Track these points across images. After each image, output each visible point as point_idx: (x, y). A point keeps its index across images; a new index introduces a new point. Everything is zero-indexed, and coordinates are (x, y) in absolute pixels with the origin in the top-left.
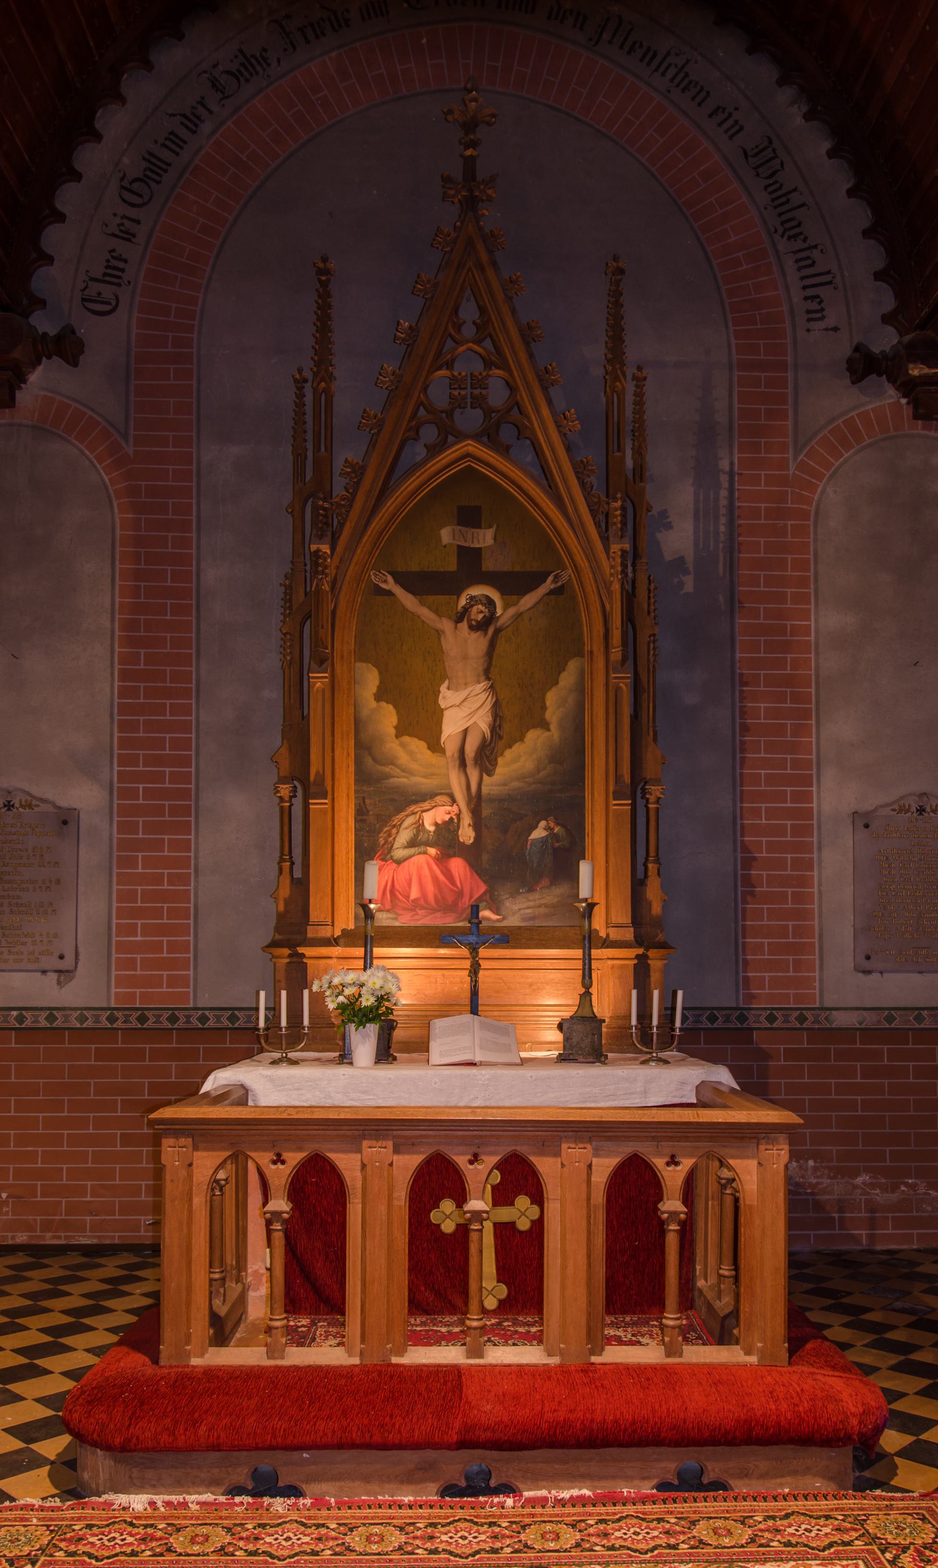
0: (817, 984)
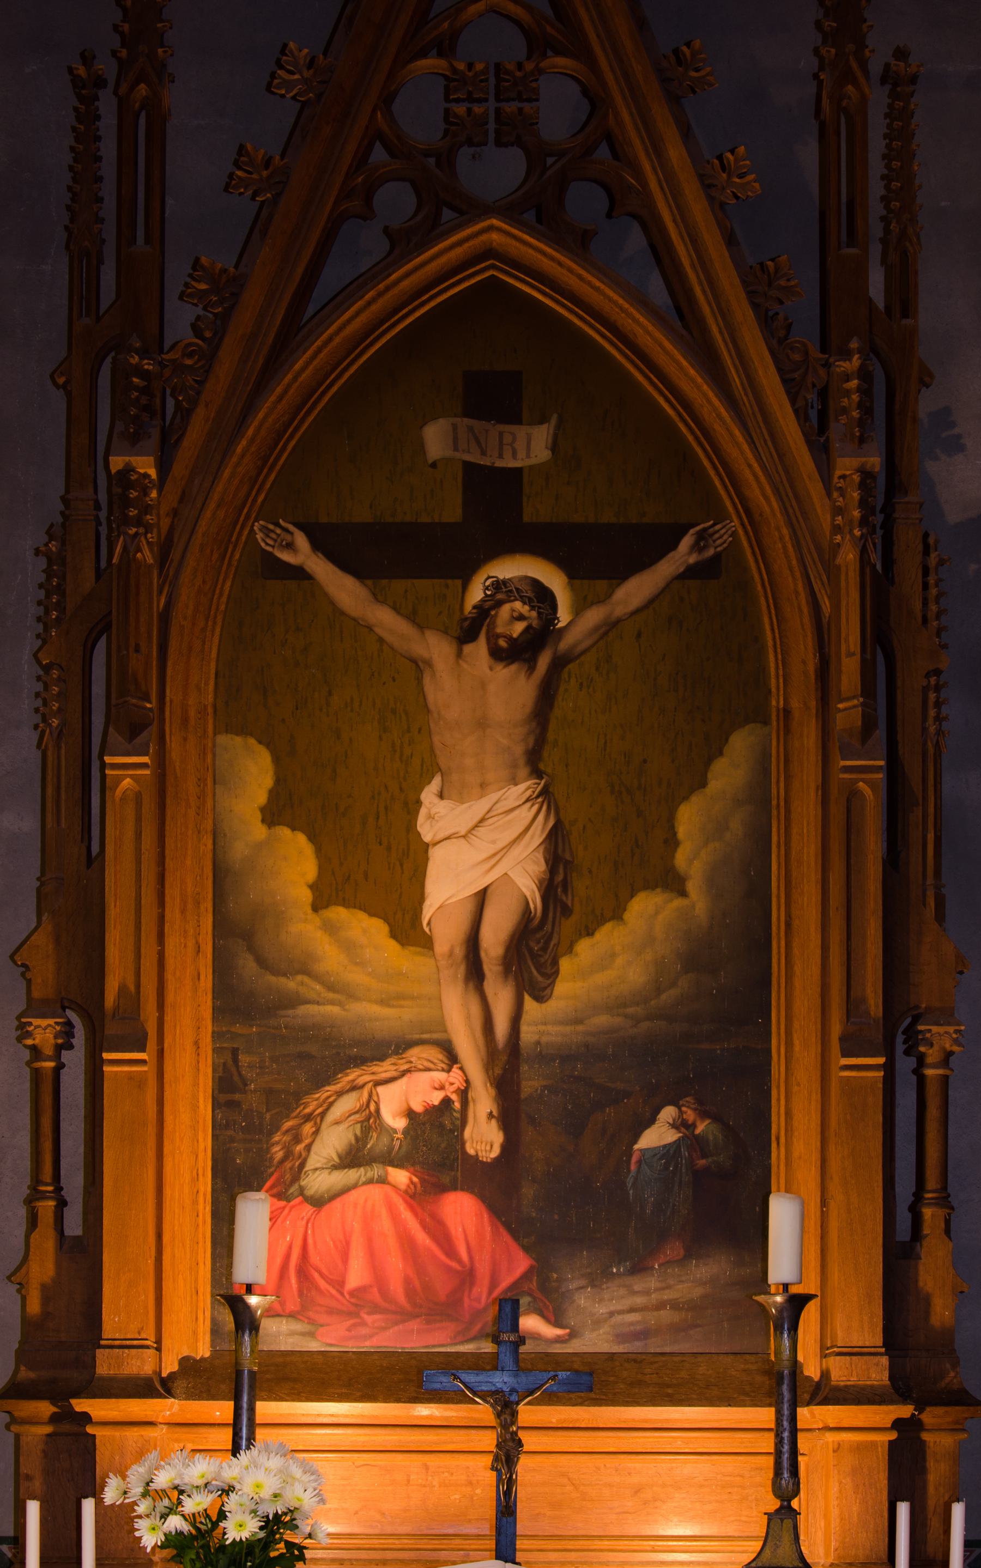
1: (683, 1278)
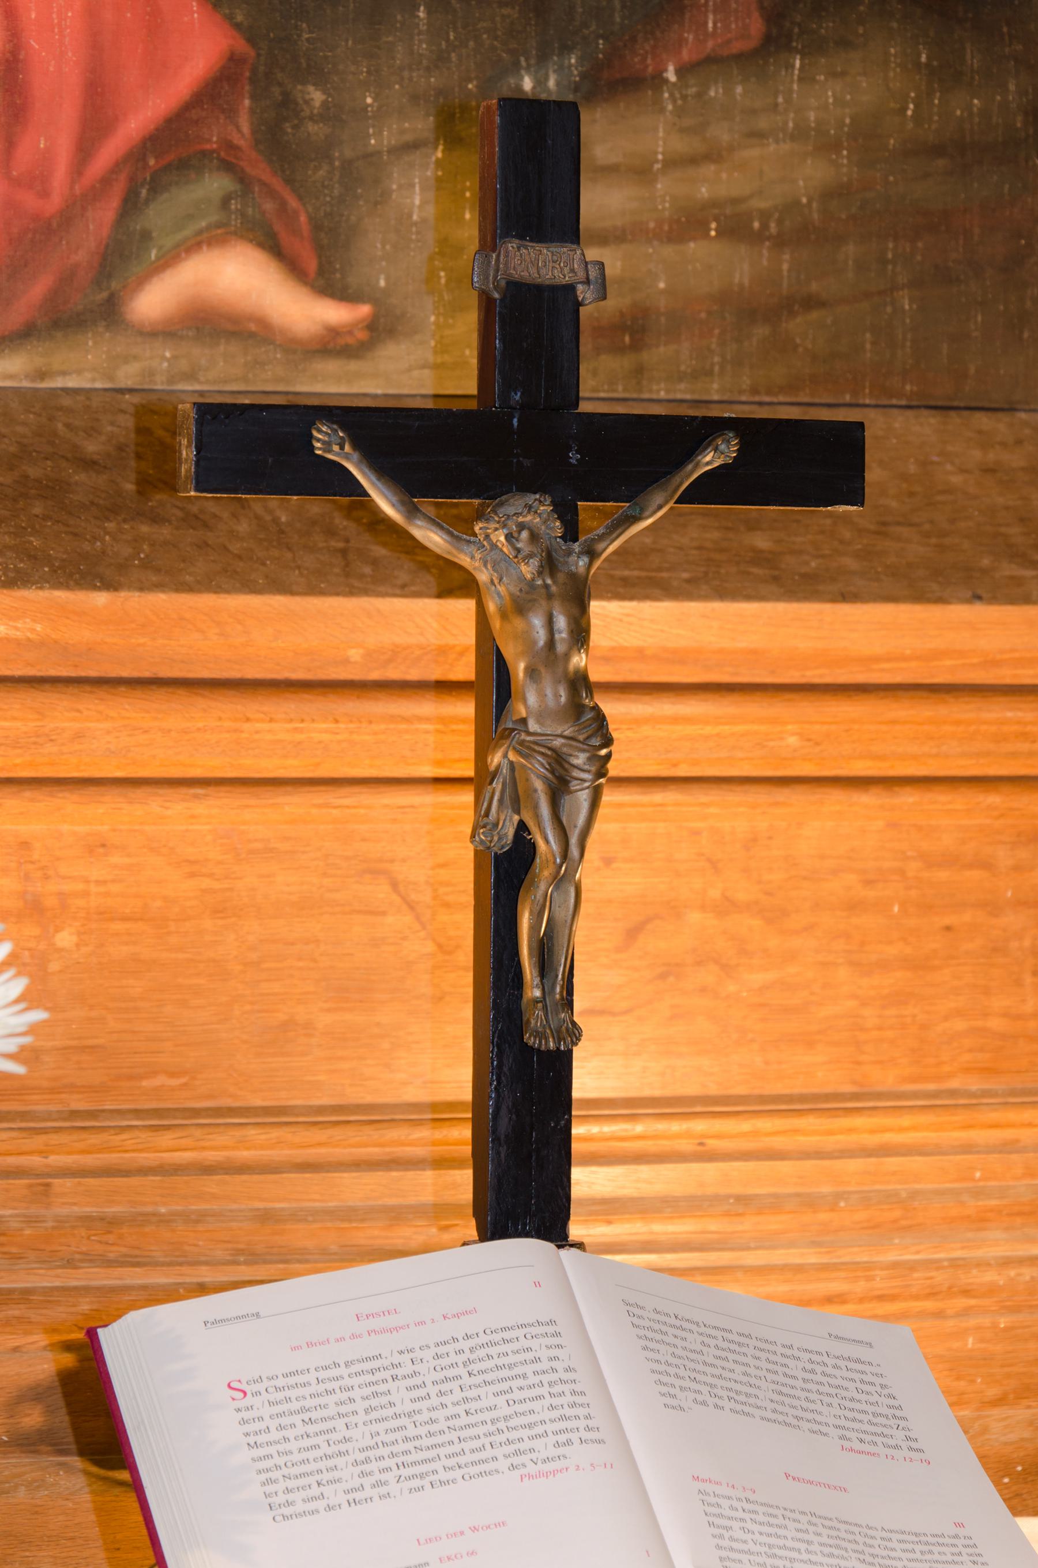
1: (763, 123)
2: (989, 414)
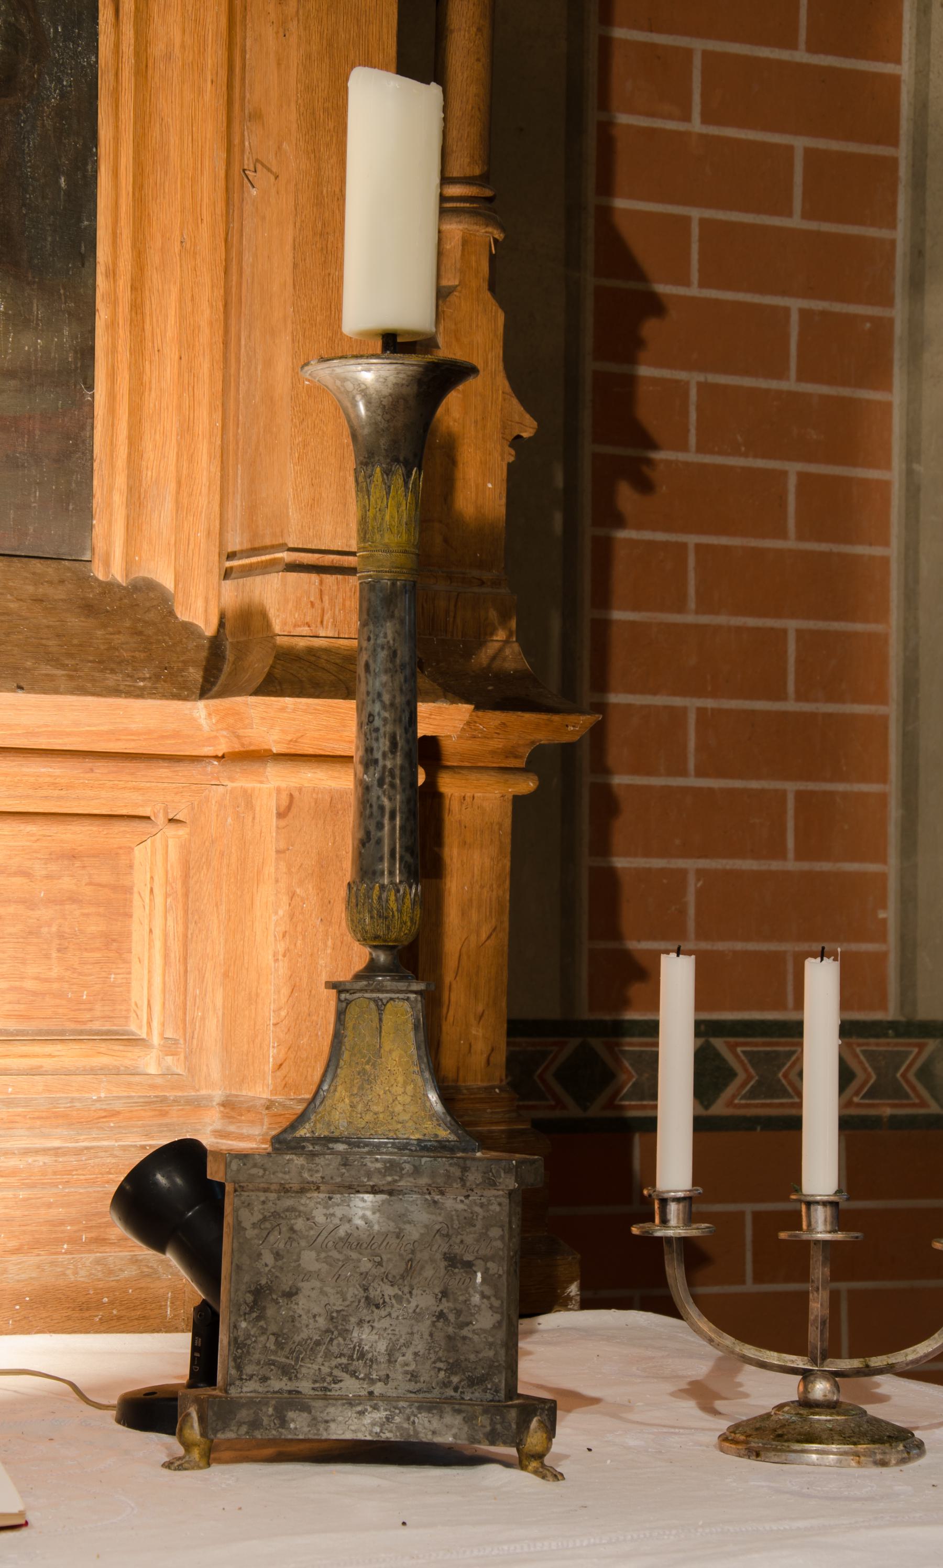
0: (890, 914)
2: (42, 561)
